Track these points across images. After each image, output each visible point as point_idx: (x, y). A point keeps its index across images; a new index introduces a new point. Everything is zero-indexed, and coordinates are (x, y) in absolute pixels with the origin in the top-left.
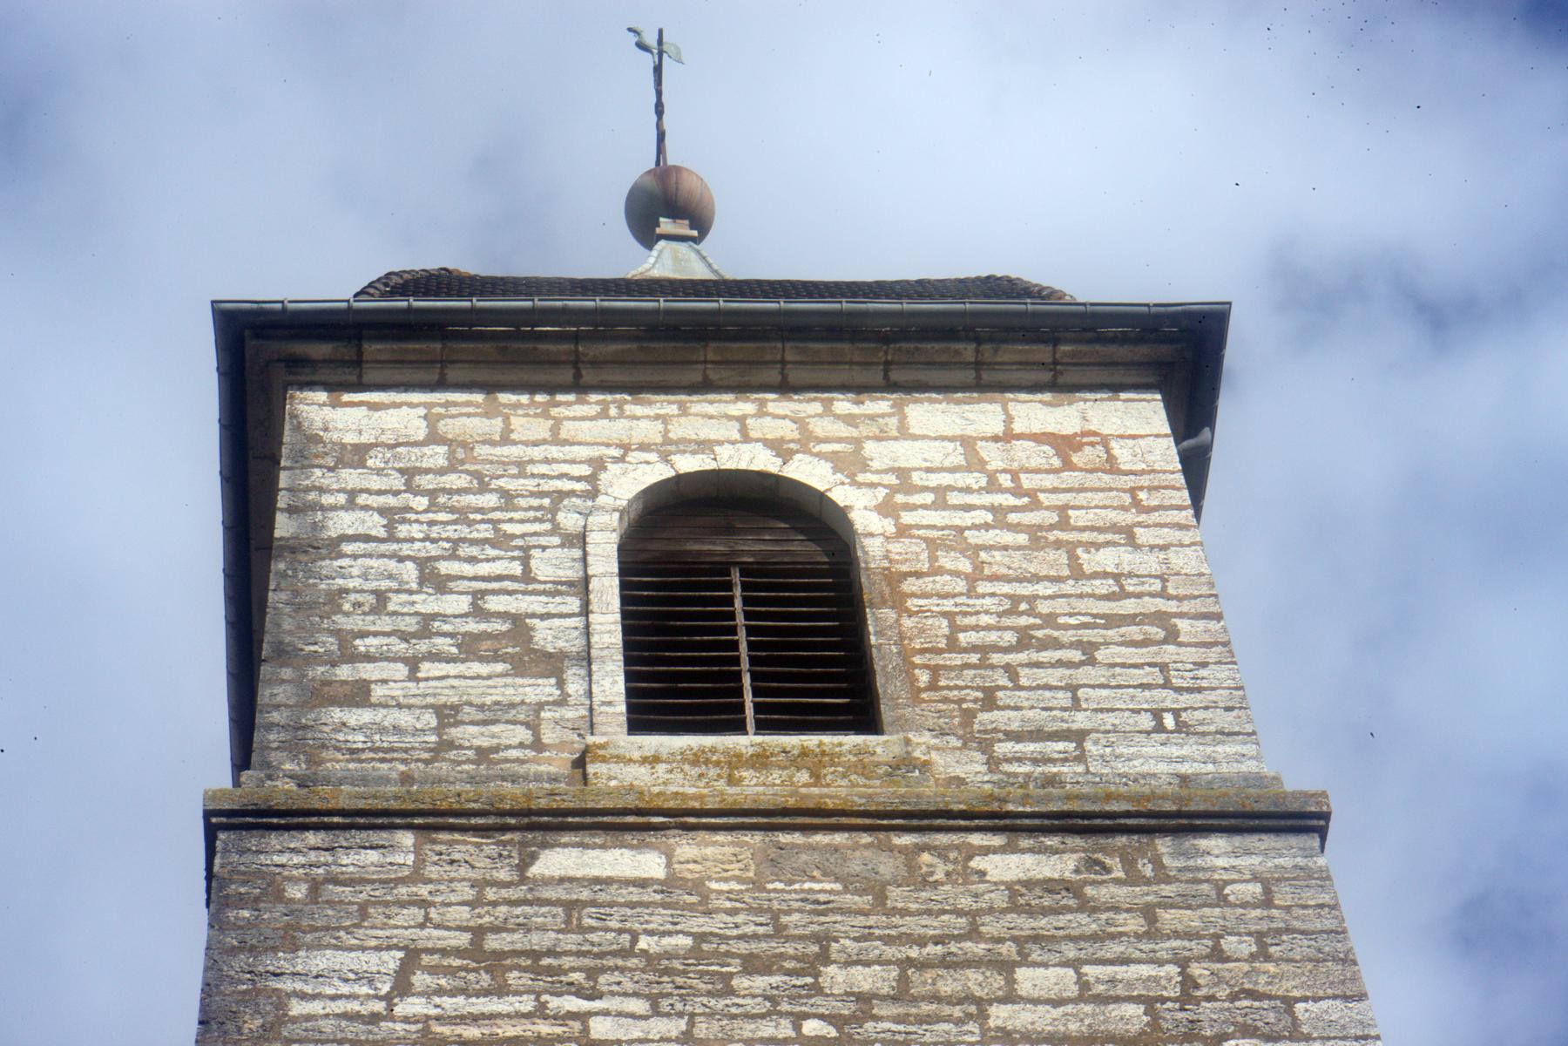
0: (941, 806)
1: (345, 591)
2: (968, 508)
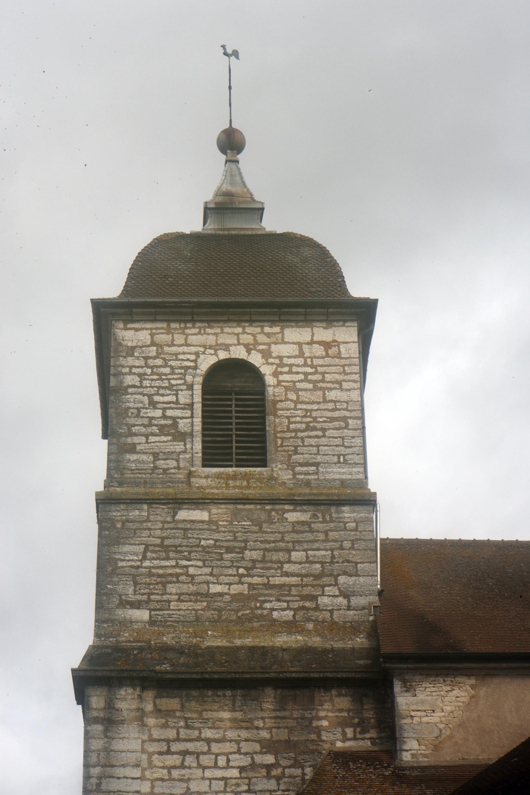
0: (278, 497)
1: (129, 408)
2: (298, 373)
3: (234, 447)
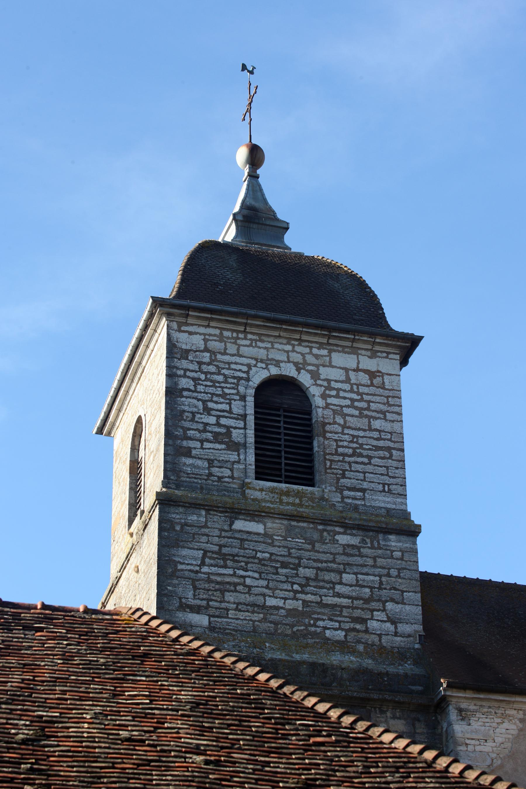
1: (184, 411)
2: (345, 398)
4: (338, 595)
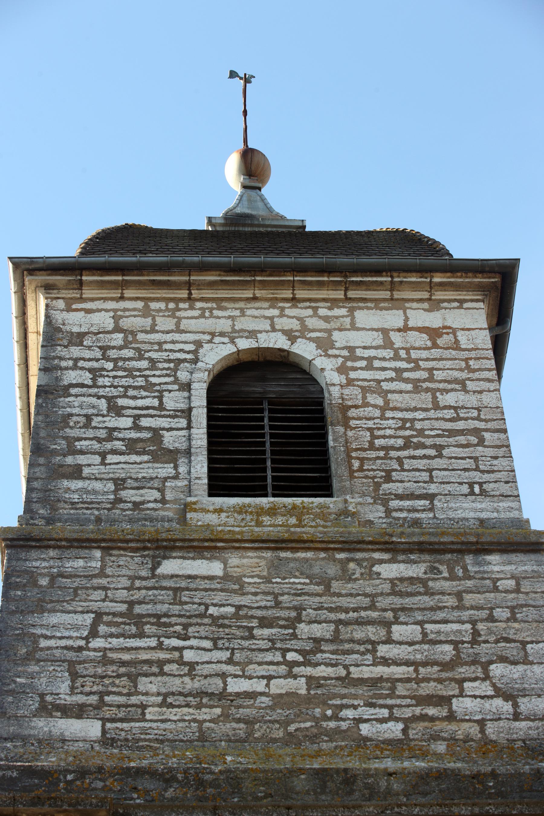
1: (72, 415)
2: (384, 369)
3: (269, 480)
4: (385, 662)
